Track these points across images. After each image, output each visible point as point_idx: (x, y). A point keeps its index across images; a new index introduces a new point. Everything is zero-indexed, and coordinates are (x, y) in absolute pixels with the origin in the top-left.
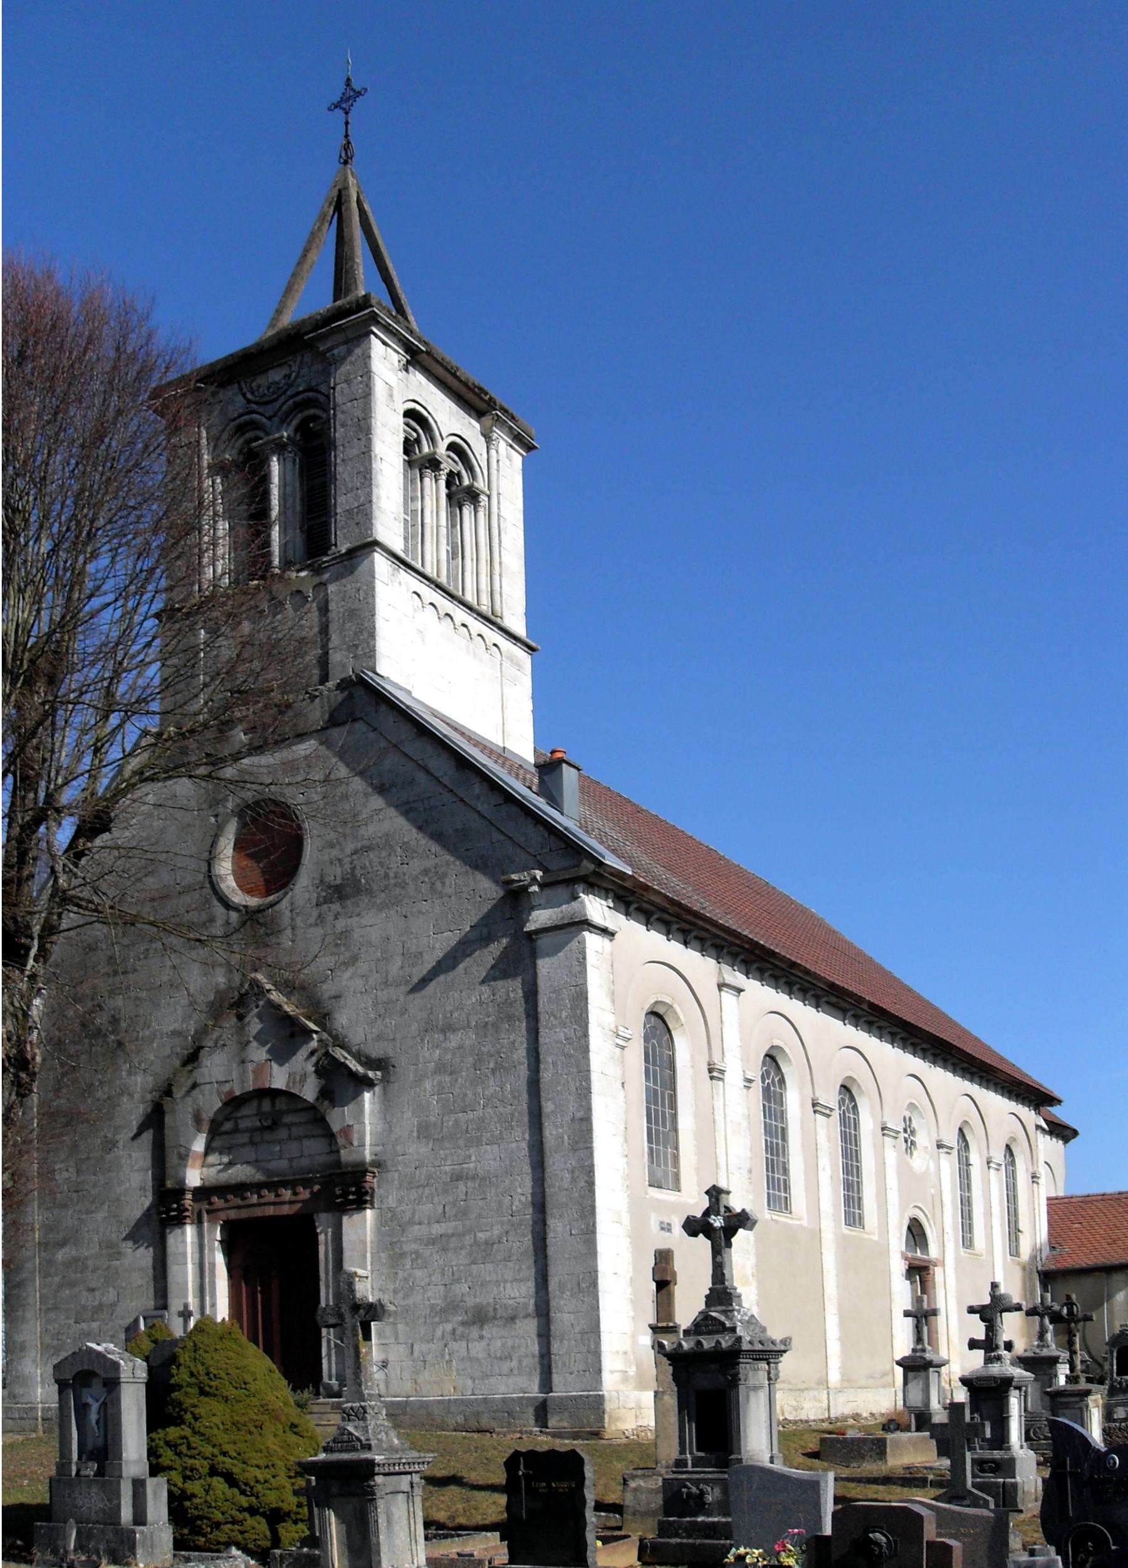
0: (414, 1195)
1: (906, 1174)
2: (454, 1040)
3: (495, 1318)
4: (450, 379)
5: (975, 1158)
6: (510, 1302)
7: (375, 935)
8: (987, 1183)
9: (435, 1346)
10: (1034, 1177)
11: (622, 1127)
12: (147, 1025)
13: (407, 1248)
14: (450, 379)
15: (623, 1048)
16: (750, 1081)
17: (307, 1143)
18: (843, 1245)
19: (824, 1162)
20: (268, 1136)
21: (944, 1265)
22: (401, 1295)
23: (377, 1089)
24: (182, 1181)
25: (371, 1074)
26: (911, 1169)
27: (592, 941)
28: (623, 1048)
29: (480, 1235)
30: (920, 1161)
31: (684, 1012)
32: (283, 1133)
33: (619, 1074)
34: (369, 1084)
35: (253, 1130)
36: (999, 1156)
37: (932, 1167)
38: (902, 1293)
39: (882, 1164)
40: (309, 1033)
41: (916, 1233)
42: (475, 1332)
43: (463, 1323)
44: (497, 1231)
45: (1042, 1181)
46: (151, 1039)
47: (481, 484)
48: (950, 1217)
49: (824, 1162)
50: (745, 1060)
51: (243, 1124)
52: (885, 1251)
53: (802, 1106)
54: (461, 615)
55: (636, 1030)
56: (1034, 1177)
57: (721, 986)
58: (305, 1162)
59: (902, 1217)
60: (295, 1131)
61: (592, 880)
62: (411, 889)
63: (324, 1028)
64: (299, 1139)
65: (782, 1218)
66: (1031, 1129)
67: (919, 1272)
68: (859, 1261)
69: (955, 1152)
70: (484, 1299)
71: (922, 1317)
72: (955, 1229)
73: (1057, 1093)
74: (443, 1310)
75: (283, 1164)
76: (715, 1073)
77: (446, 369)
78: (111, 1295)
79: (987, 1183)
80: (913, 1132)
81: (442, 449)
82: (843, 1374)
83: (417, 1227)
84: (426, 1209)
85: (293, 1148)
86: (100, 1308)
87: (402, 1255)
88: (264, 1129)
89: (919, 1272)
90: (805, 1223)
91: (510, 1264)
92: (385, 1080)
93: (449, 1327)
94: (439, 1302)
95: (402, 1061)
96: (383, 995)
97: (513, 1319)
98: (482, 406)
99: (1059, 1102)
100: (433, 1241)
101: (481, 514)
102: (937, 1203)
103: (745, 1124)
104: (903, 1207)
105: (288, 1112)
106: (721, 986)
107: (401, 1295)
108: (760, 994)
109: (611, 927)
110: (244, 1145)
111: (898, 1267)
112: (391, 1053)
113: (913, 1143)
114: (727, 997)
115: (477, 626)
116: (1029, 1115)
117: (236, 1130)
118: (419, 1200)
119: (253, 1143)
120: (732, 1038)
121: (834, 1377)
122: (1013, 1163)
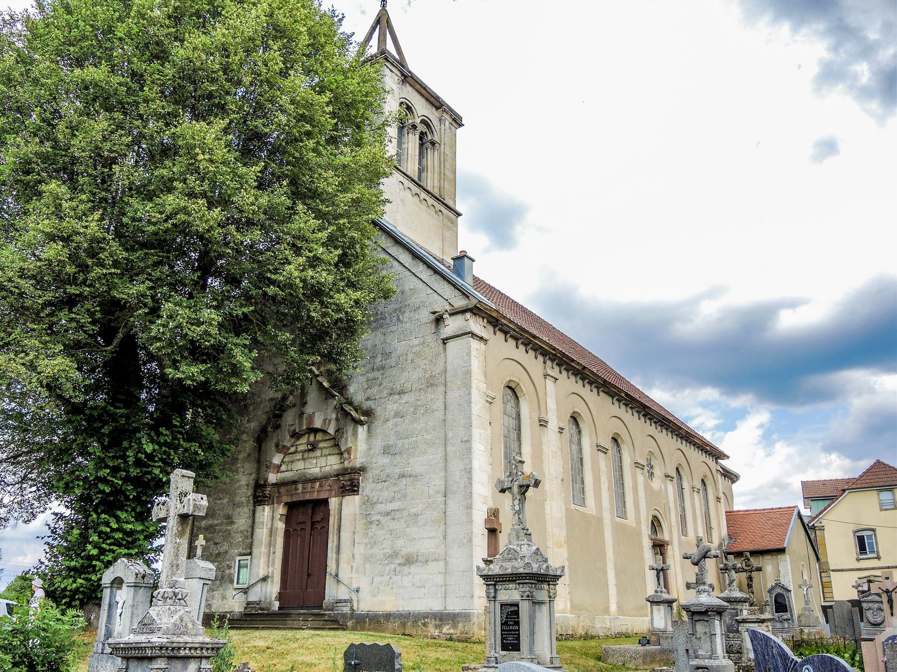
0: (380, 486)
1: (647, 488)
2: (405, 398)
3: (417, 561)
4: (423, 91)
5: (686, 485)
6: (426, 551)
7: (369, 344)
8: (692, 499)
9: (386, 578)
10: (718, 499)
11: (489, 447)
12: (259, 396)
13: (374, 518)
14: (423, 91)
15: (491, 403)
16: (562, 429)
17: (329, 457)
18: (617, 528)
19: (604, 479)
20: (311, 454)
21: (672, 545)
22: (369, 546)
23: (365, 426)
24: (266, 480)
25: (362, 418)
26: (651, 487)
27: (475, 344)
28: (491, 403)
29: (412, 510)
30: (656, 484)
31: (525, 387)
32: (318, 453)
33: (488, 417)
34: (362, 423)
35: (304, 451)
36: (699, 485)
37: (663, 487)
38: (649, 557)
39: (635, 483)
40: (334, 396)
41: (656, 524)
42: (406, 569)
43: (400, 564)
44: (420, 507)
45: (722, 501)
46: (261, 403)
47: (436, 139)
48: (674, 518)
49: (604, 479)
50: (559, 418)
51: (301, 448)
52: (639, 534)
53: (591, 446)
54: (423, 195)
55: (499, 392)
56: (718, 499)
57: (546, 376)
58: (328, 469)
59: (648, 513)
60: (326, 452)
61: (475, 311)
62: (388, 319)
63: (342, 395)
64: (326, 456)
65: (580, 509)
66: (714, 472)
67: (659, 547)
68: (624, 534)
69: (675, 480)
70: (410, 549)
71: (661, 573)
72: (677, 523)
73: (726, 452)
74: (391, 556)
75: (317, 470)
76: (543, 423)
77: (421, 86)
78: (225, 547)
79: (692, 499)
80: (652, 467)
81: (418, 121)
82: (618, 607)
83: (380, 505)
84: (386, 494)
85: (322, 461)
86: (219, 554)
87: (371, 523)
88: (310, 450)
89: (659, 547)
90: (594, 514)
91: (427, 528)
92: (370, 424)
93: (393, 566)
94: (388, 551)
95: (379, 411)
96: (371, 375)
97: (427, 561)
98: (438, 104)
99: (728, 457)
100: (388, 514)
101: (436, 152)
102: (667, 508)
103: (559, 453)
104: (648, 510)
105: (321, 441)
106: (546, 376)
107: (369, 546)
108: (569, 383)
109: (485, 336)
110: (298, 460)
111: (647, 544)
112: (373, 407)
113: (652, 473)
114: (549, 383)
115: (431, 201)
116: (710, 461)
117: (296, 452)
118: (381, 490)
119: (303, 459)
120: (551, 404)
121: (613, 607)
122: (706, 490)
